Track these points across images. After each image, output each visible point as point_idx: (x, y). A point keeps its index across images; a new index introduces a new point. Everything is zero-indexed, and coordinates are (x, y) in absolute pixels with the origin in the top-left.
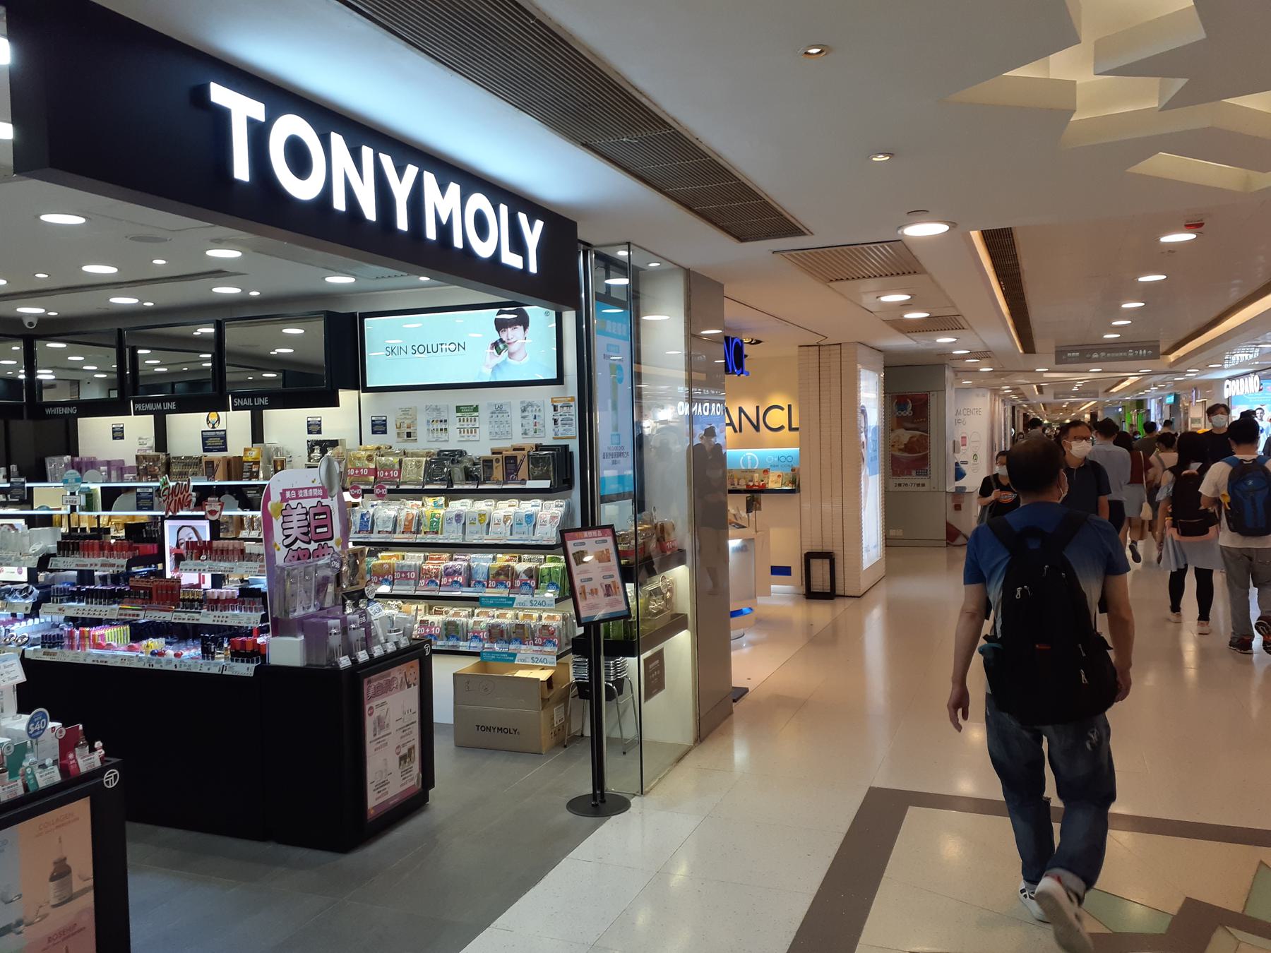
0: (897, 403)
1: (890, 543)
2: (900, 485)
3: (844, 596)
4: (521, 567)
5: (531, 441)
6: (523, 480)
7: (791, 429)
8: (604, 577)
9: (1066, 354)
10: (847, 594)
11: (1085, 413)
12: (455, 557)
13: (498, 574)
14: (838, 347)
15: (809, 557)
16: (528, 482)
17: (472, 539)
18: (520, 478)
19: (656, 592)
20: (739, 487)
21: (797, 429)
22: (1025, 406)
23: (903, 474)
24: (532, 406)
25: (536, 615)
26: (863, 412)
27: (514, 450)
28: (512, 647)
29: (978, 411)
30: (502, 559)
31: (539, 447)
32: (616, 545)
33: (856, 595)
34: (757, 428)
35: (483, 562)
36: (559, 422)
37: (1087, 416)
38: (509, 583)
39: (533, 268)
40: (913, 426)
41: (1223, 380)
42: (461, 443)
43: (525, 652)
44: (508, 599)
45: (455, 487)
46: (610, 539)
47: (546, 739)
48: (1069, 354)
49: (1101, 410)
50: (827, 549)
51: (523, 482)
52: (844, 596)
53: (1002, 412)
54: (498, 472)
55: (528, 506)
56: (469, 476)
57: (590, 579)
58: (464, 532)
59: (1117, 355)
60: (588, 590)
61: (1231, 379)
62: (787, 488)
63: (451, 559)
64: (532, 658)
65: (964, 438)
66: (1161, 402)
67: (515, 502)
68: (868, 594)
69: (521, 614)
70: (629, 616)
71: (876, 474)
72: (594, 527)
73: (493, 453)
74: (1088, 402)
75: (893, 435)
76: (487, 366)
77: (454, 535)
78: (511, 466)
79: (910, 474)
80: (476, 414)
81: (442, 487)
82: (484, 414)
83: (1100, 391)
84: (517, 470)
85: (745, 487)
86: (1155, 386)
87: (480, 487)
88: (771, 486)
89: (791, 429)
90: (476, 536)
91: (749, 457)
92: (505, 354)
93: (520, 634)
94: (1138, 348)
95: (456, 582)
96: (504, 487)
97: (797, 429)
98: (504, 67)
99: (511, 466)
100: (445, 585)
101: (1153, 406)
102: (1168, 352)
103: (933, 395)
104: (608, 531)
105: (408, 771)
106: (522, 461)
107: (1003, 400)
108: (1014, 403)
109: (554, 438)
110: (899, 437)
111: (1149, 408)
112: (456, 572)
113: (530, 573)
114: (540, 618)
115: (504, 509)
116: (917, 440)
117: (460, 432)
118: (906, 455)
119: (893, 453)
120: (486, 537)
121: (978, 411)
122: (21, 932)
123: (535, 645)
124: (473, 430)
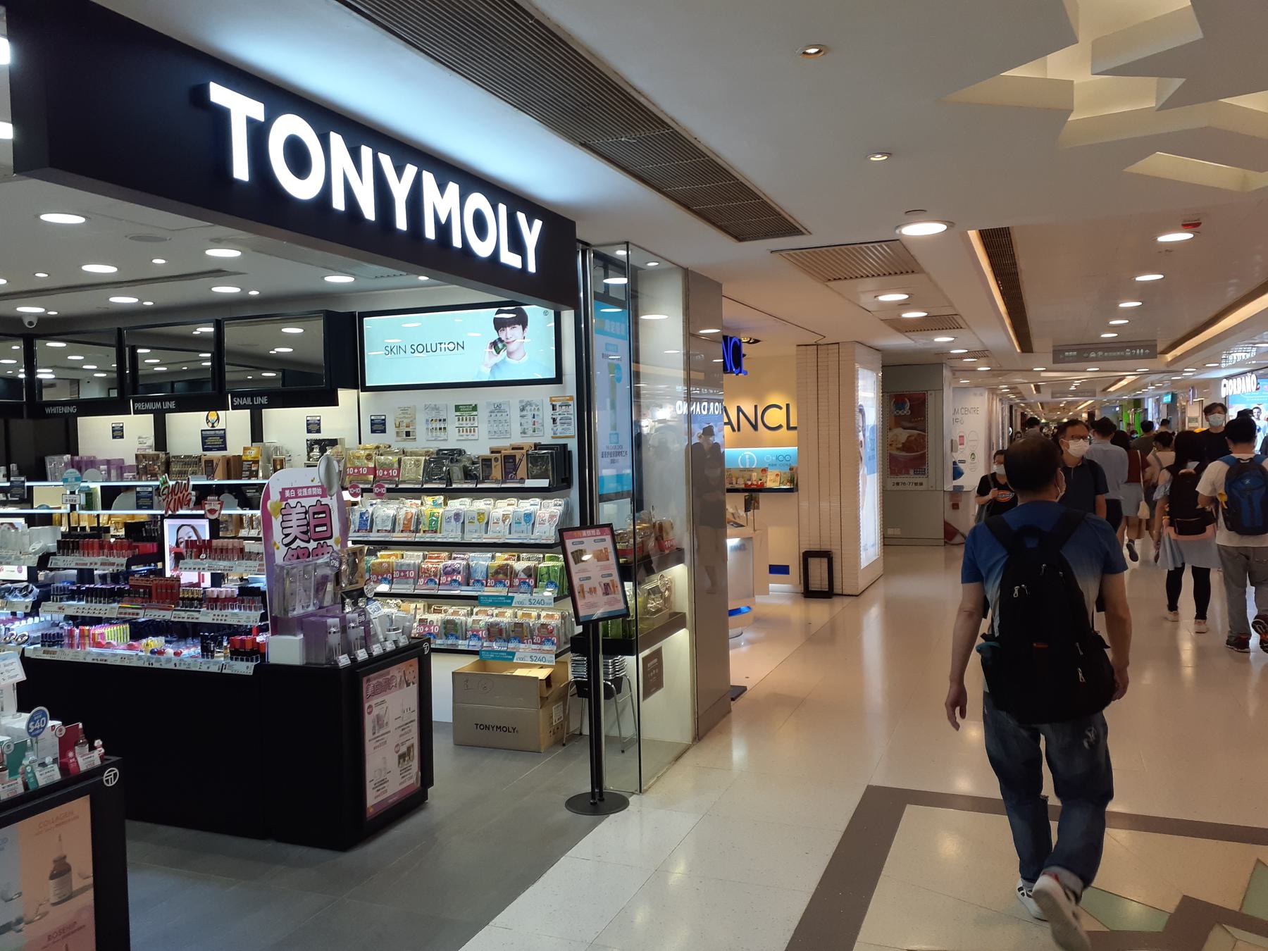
0: (895, 402)
1: (888, 542)
2: (898, 484)
3: (842, 595)
4: (520, 566)
5: (530, 440)
6: (522, 479)
7: (789, 428)
8: (603, 576)
9: (1064, 354)
10: (845, 593)
11: (1083, 412)
12: (454, 555)
13: (497, 572)
14: (836, 346)
15: (807, 556)
16: (527, 481)
17: (471, 538)
18: (519, 477)
19: (655, 591)
20: (737, 486)
21: (795, 428)
22: (1022, 405)
23: (901, 473)
24: (531, 405)
25: (534, 614)
26: (861, 411)
27: (513, 449)
28: (511, 645)
29: (975, 410)
30: (501, 558)
31: (538, 446)
32: (614, 543)
33: (854, 593)
34: (755, 427)
35: (481, 561)
36: (558, 421)
37: (1085, 416)
38: (508, 582)
39: (532, 268)
40: (911, 425)
41: (1220, 379)
42: (460, 442)
43: (524, 650)
44: (507, 597)
45: (454, 486)
46: (608, 538)
47: (545, 737)
48: (1067, 354)
49: (1099, 409)
50: (825, 547)
51: (522, 480)
52: (842, 595)
53: (1000, 411)
54: (497, 471)
55: (527, 505)
56: (468, 475)
57: (589, 578)
58: (463, 531)
59: (1114, 354)
60: (586, 589)
61: (1228, 378)
62: (785, 487)
63: (450, 558)
64: (531, 657)
65: (962, 437)
66: (1158, 401)
67: (513, 501)
68: (866, 593)
69: (520, 613)
70: (628, 615)
71: (874, 473)
72: (593, 526)
73: (492, 452)
74: (1086, 402)
75: (890, 434)
76: (486, 365)
77: (453, 534)
78: (510, 465)
79: (908, 473)
80: (475, 413)
81: (441, 486)
82: (483, 413)
83: (1097, 390)
84: (515, 469)
85: (743, 486)
86: (1152, 385)
87: (479, 486)
88: (769, 485)
89: (789, 428)
90: (475, 535)
91: (747, 456)
92: (503, 354)
93: (519, 632)
94: (1135, 348)
95: (455, 581)
96: (503, 486)
97: (795, 428)
98: (503, 66)
99: (510, 465)
100: (444, 584)
101: (1150, 405)
102: (1166, 352)
103: (931, 394)
104: (607, 530)
105: (407, 769)
106: (521, 460)
107: (1000, 400)
108: (1012, 402)
109: (552, 437)
110: (897, 436)
111: (1146, 407)
112: (455, 571)
113: (529, 572)
114: (539, 616)
115: (503, 508)
116: (915, 439)
117: (459, 431)
118: (904, 454)
119: (891, 452)
120: (485, 536)
121: (975, 410)
122: (21, 930)
123: (533, 643)
124: (472, 429)
